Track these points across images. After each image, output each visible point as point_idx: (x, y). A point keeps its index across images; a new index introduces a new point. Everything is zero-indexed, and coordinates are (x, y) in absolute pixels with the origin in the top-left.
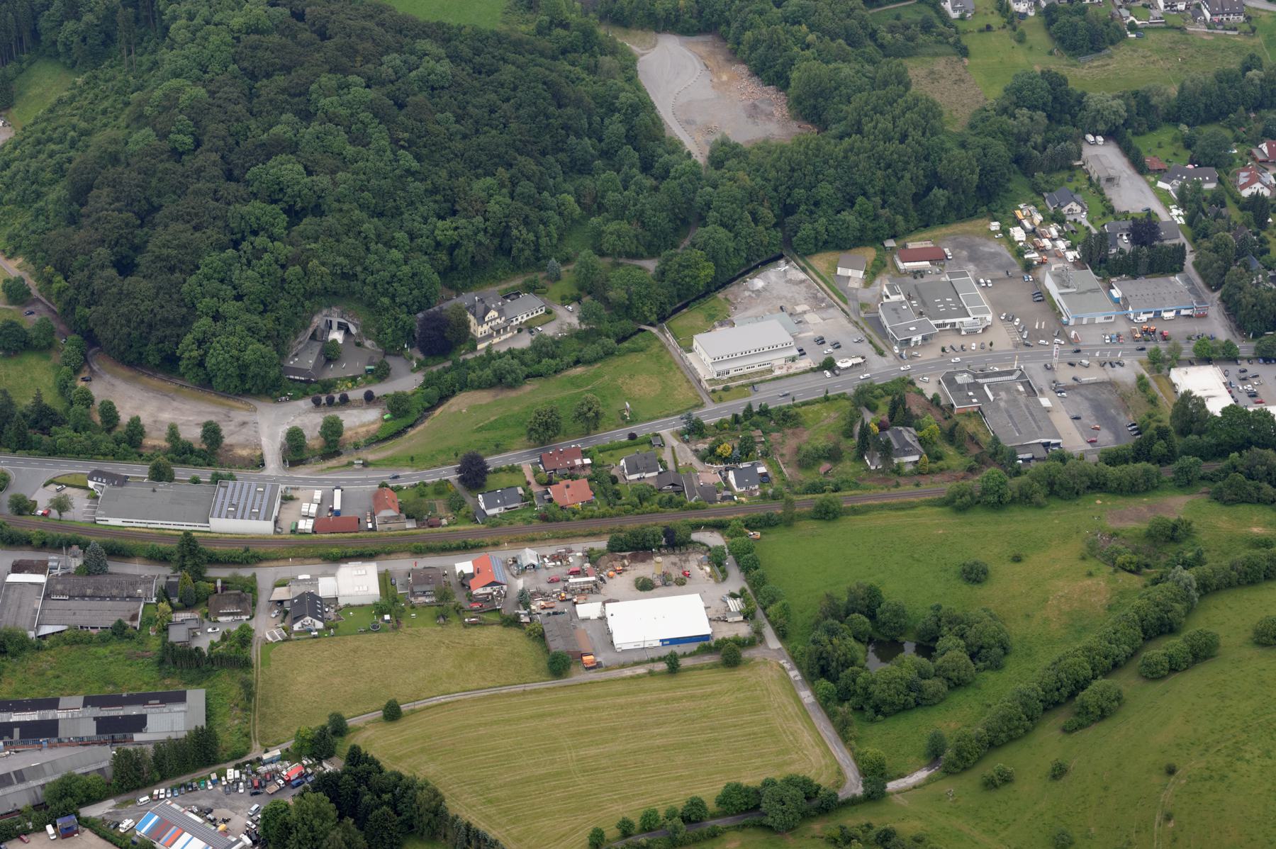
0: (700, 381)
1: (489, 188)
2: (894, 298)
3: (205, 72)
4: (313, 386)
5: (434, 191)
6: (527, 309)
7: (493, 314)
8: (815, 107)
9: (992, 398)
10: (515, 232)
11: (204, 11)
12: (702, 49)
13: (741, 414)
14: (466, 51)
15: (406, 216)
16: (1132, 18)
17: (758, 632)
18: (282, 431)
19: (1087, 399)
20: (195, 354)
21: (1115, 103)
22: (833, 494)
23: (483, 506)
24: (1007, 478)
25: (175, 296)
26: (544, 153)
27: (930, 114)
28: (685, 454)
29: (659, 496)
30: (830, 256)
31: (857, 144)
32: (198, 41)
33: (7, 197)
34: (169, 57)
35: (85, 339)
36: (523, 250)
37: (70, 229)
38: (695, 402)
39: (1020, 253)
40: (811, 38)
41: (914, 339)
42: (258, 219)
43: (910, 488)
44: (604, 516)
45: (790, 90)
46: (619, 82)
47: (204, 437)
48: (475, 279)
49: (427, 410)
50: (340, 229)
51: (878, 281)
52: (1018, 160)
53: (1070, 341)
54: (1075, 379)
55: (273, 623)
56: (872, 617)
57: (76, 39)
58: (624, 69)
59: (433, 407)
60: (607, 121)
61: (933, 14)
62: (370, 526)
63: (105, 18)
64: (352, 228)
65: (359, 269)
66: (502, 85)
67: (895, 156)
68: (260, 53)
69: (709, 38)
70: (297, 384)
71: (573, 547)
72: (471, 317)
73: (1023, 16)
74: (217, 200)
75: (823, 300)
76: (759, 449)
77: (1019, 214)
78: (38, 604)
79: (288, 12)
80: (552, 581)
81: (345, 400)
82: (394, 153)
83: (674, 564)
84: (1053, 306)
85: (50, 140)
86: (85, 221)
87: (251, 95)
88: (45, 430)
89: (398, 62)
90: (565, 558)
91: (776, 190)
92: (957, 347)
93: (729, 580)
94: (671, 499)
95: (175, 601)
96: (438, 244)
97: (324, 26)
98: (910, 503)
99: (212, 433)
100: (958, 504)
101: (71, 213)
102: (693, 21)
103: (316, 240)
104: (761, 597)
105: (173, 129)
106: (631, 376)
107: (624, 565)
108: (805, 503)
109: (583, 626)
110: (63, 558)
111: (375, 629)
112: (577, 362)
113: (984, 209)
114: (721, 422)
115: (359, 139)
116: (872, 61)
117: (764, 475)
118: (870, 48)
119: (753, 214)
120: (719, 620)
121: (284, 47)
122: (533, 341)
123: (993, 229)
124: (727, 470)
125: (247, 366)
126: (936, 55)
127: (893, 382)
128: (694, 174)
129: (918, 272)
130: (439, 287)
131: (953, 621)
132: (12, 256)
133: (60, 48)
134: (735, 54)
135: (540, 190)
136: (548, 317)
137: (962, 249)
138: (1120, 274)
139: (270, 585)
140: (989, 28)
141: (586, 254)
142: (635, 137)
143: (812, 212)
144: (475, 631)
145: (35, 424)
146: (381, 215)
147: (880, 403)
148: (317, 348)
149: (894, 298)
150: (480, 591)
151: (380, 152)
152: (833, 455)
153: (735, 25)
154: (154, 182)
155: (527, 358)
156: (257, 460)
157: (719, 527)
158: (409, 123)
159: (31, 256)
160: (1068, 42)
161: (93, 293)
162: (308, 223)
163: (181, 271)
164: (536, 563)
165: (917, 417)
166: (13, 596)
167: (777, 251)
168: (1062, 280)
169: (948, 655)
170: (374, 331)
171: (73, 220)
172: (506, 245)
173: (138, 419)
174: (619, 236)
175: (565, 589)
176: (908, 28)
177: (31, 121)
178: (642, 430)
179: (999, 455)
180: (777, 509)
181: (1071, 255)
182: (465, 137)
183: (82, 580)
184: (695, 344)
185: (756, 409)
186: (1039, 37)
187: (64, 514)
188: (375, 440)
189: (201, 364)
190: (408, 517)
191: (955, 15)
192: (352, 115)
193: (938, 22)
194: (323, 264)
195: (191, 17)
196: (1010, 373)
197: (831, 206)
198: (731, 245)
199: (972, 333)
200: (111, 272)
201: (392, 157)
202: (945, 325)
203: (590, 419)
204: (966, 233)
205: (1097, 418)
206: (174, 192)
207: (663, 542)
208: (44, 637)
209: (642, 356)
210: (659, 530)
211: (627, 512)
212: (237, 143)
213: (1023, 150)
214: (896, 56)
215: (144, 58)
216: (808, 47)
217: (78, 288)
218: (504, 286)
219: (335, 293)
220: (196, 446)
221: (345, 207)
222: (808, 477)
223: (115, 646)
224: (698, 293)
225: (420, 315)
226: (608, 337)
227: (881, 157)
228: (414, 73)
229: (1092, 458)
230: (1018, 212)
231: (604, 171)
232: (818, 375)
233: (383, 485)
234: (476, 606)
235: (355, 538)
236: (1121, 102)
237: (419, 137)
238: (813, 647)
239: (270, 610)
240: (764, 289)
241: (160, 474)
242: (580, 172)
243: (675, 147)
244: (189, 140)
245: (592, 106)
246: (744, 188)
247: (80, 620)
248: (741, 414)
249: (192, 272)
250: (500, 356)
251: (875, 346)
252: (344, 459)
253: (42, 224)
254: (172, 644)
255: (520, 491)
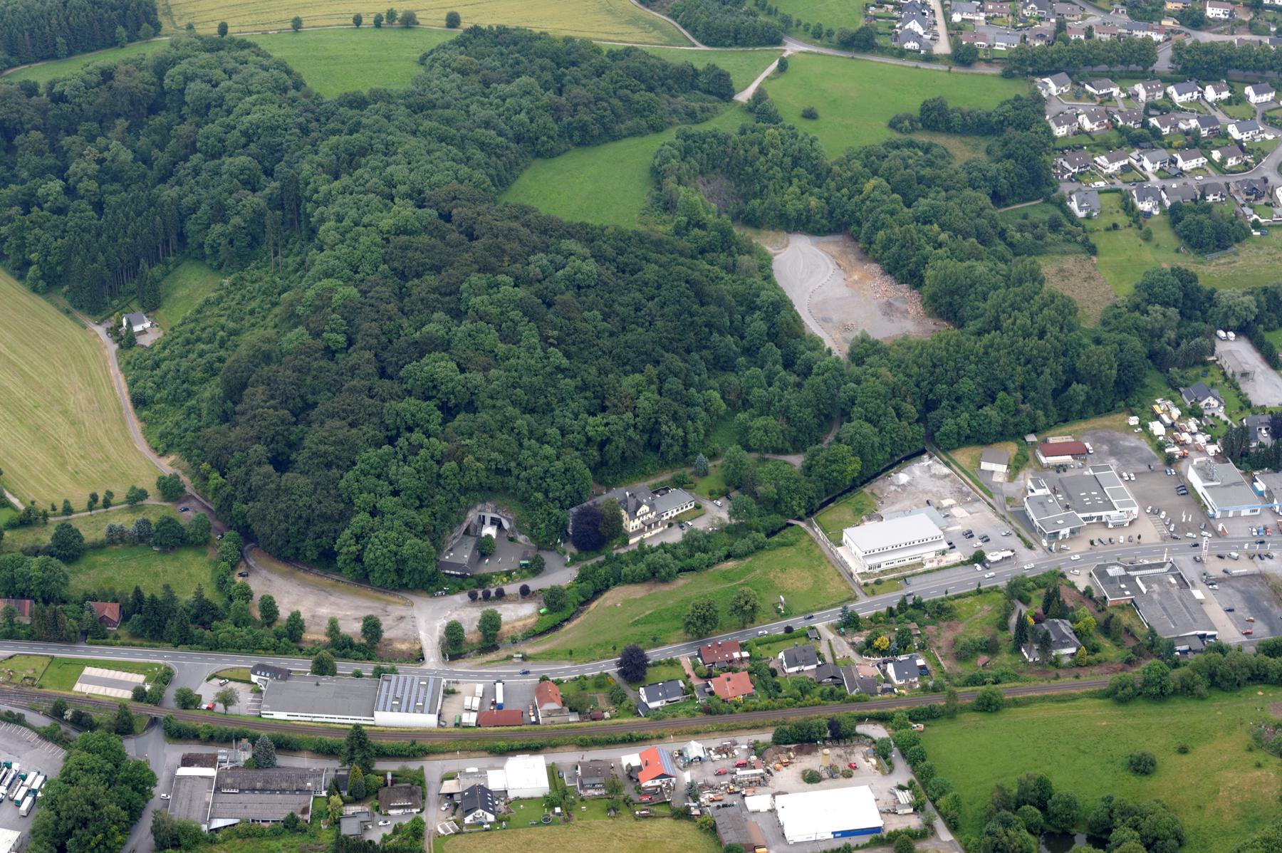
0: (851, 575)
1: (638, 385)
2: (1039, 492)
3: (356, 272)
4: (469, 580)
5: (584, 387)
6: (677, 504)
7: (645, 508)
8: (951, 304)
9: (1144, 590)
10: (664, 428)
11: (353, 213)
12: (834, 249)
13: (895, 607)
14: (610, 252)
15: (557, 412)
16: (1255, 217)
17: (929, 825)
18: (440, 625)
19: (1239, 591)
20: (353, 548)
21: (1247, 299)
22: (994, 687)
23: (645, 699)
24: (1168, 669)
25: (332, 492)
26: (688, 351)
27: (1066, 311)
28: (842, 648)
29: (819, 689)
30: (974, 451)
31: (997, 340)
32: (348, 242)
33: (158, 395)
34: (320, 260)
35: (241, 535)
36: (672, 445)
37: (225, 426)
38: (847, 596)
39: (1160, 447)
40: (943, 237)
41: (1062, 532)
42: (413, 415)
43: (1069, 680)
44: (767, 709)
45: (924, 288)
46: (758, 280)
47: (365, 631)
48: (625, 474)
49: (582, 604)
50: (494, 426)
51: (1021, 475)
52: (1152, 356)
53: (1217, 534)
54: (1225, 571)
55: (443, 816)
56: (1043, 808)
57: (224, 241)
58: (761, 267)
59: (588, 601)
60: (748, 319)
61: (1060, 213)
62: (533, 719)
63: (252, 221)
64: (506, 424)
65: (513, 464)
66: (646, 284)
67: (1035, 352)
68: (410, 254)
69: (839, 238)
70: (453, 579)
71: (738, 739)
72: (623, 512)
73: (1149, 214)
74: (372, 397)
75: (968, 494)
76: (916, 642)
77: (1158, 409)
78: (209, 797)
79: (435, 213)
80: (719, 774)
81: (500, 595)
82: (544, 351)
83: (840, 756)
84: (1198, 500)
85: (199, 340)
86: (242, 419)
87: (401, 294)
88: (205, 625)
89: (545, 261)
90: (731, 750)
91: (918, 385)
92: (1105, 539)
93: (896, 772)
94: (832, 692)
95: (345, 794)
96: (589, 440)
97: (471, 227)
98: (1070, 695)
99: (372, 628)
100: (1119, 696)
101: (224, 411)
102: (824, 221)
103: (471, 436)
104: (928, 788)
105: (326, 328)
106: (783, 570)
107: (789, 758)
108: (968, 694)
109: (753, 818)
110: (232, 751)
111: (546, 821)
112: (728, 557)
113: (1122, 404)
114: (876, 615)
115: (510, 337)
116: (1003, 259)
117: (923, 667)
118: (1001, 247)
119: (897, 409)
120: (888, 812)
121: (434, 247)
122: (684, 536)
123: (1132, 423)
124: (885, 663)
125: (404, 561)
126: (1064, 253)
127: (1044, 575)
128: (837, 369)
129: (1061, 466)
130: (591, 482)
131: (1126, 812)
132: (164, 453)
133: (207, 251)
134: (867, 253)
135: (687, 386)
136: (697, 512)
137: (1103, 443)
138: (1262, 468)
139: (438, 779)
140: (1115, 226)
141: (734, 449)
142: (777, 334)
143: (953, 408)
144: (647, 824)
145: (196, 618)
146: (532, 411)
147: (1032, 595)
148: (471, 543)
149: (1039, 492)
150: (649, 783)
151: (531, 349)
152: (990, 648)
153: (866, 225)
154: (309, 380)
155: (679, 552)
156: (417, 655)
157: (881, 719)
158: (559, 321)
159: (187, 454)
160: (1194, 240)
161: (250, 489)
162: (461, 419)
163: (338, 467)
164: (702, 755)
165: (1072, 609)
166: (184, 790)
167: (921, 446)
168: (1206, 474)
169: (1125, 846)
170: (527, 525)
171: (225, 417)
172: (655, 440)
173: (298, 613)
174: (766, 431)
175: (733, 782)
176: (1036, 227)
177: (179, 322)
178: (798, 623)
179: (1153, 646)
180: (940, 702)
181: (1212, 449)
182: (612, 334)
183: (252, 773)
184: (845, 537)
185: (910, 602)
186: (1165, 235)
187: (229, 708)
188: (533, 634)
189: (359, 559)
190: (571, 710)
191: (1081, 214)
192: (502, 313)
193: (1065, 221)
194: (478, 460)
195: (340, 219)
196: (1161, 565)
197: (973, 401)
198: (876, 440)
199: (1119, 526)
200: (269, 468)
201: (542, 354)
202: (1092, 518)
203: (746, 612)
204: (1104, 428)
205: (1250, 610)
206: (329, 390)
207: (828, 735)
208: (217, 830)
209: (792, 550)
210: (825, 723)
211: (789, 705)
212: (390, 341)
213: (1157, 346)
214: (1030, 255)
215: (290, 260)
216: (940, 245)
217: (235, 485)
218: (653, 481)
219: (489, 489)
220: (356, 641)
221: (499, 403)
222: (966, 670)
223: (288, 839)
224: (845, 488)
225: (574, 510)
226: (758, 531)
227: (1021, 353)
228: (561, 272)
229: (1250, 650)
230: (1156, 407)
231: (748, 368)
232: (969, 569)
233: (544, 679)
234: (646, 799)
235: (520, 731)
236: (1252, 298)
237: (568, 335)
238: (988, 839)
239: (440, 803)
240: (910, 483)
241: (323, 668)
242: (723, 369)
243: (816, 344)
244: (342, 338)
245: (734, 304)
246: (886, 384)
247: (252, 813)
248: (895, 607)
249: (348, 469)
250: (653, 551)
251: (1024, 540)
252: (503, 653)
253: (194, 422)
254: (346, 837)
255: (682, 684)
